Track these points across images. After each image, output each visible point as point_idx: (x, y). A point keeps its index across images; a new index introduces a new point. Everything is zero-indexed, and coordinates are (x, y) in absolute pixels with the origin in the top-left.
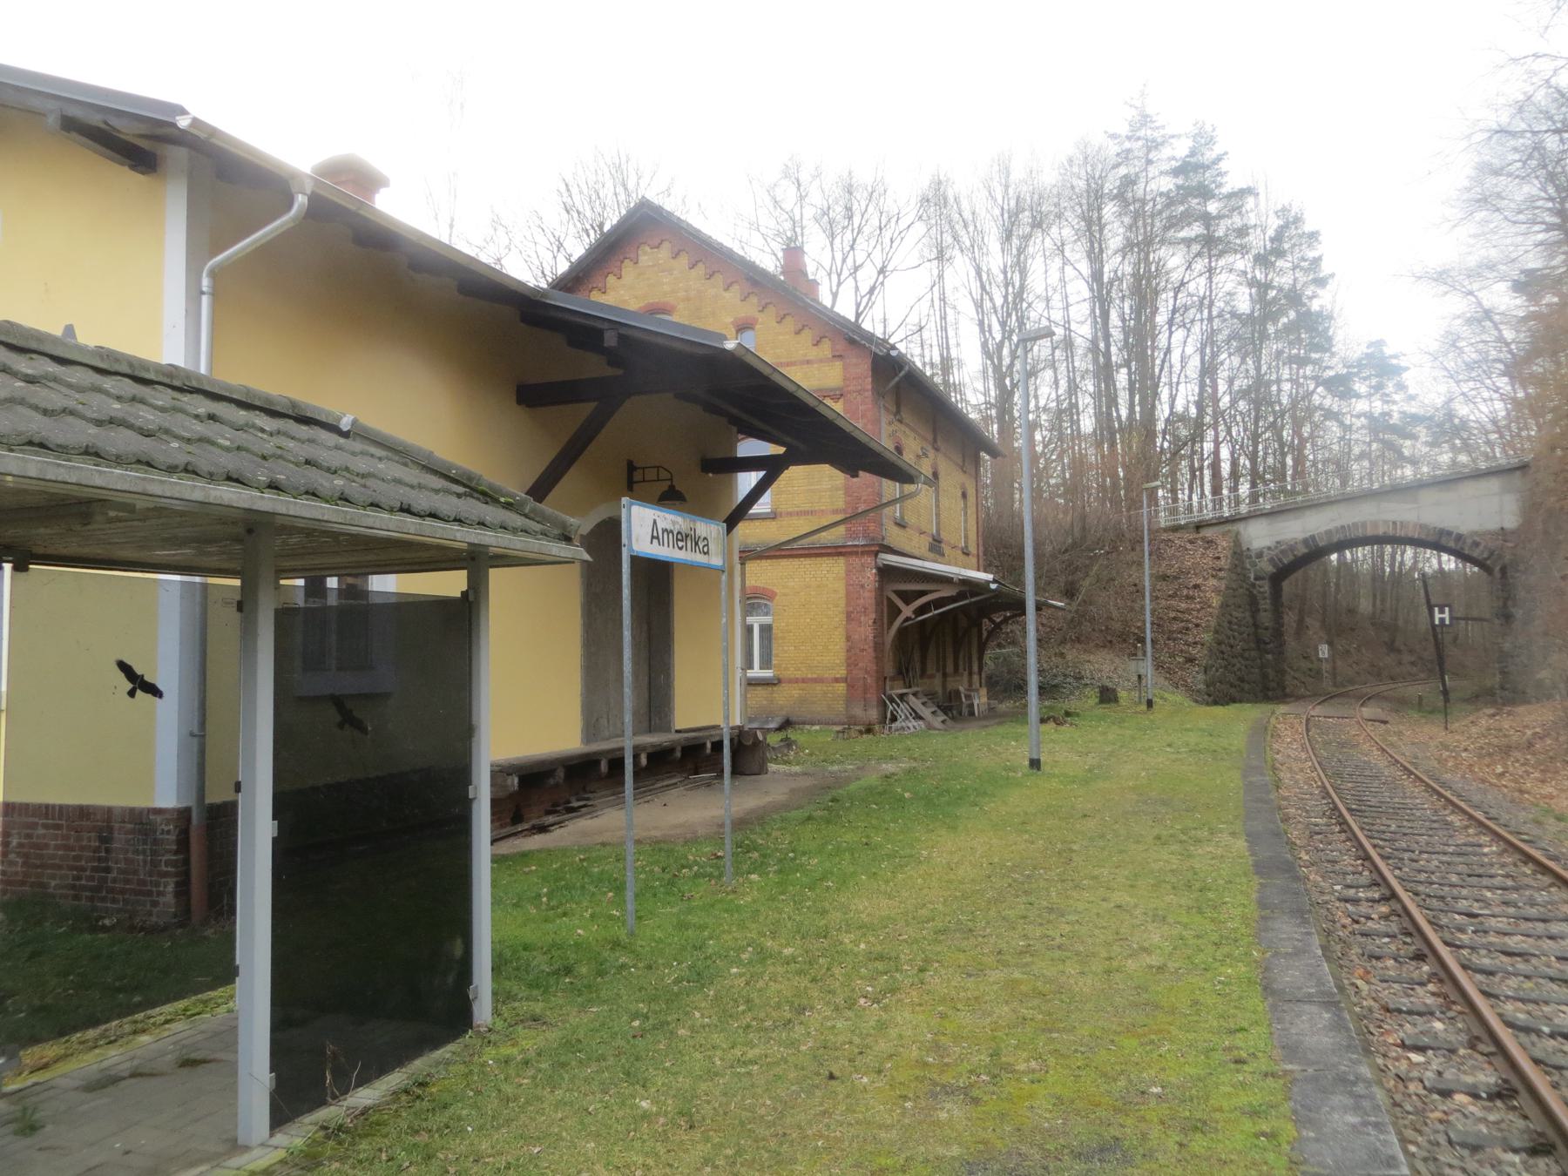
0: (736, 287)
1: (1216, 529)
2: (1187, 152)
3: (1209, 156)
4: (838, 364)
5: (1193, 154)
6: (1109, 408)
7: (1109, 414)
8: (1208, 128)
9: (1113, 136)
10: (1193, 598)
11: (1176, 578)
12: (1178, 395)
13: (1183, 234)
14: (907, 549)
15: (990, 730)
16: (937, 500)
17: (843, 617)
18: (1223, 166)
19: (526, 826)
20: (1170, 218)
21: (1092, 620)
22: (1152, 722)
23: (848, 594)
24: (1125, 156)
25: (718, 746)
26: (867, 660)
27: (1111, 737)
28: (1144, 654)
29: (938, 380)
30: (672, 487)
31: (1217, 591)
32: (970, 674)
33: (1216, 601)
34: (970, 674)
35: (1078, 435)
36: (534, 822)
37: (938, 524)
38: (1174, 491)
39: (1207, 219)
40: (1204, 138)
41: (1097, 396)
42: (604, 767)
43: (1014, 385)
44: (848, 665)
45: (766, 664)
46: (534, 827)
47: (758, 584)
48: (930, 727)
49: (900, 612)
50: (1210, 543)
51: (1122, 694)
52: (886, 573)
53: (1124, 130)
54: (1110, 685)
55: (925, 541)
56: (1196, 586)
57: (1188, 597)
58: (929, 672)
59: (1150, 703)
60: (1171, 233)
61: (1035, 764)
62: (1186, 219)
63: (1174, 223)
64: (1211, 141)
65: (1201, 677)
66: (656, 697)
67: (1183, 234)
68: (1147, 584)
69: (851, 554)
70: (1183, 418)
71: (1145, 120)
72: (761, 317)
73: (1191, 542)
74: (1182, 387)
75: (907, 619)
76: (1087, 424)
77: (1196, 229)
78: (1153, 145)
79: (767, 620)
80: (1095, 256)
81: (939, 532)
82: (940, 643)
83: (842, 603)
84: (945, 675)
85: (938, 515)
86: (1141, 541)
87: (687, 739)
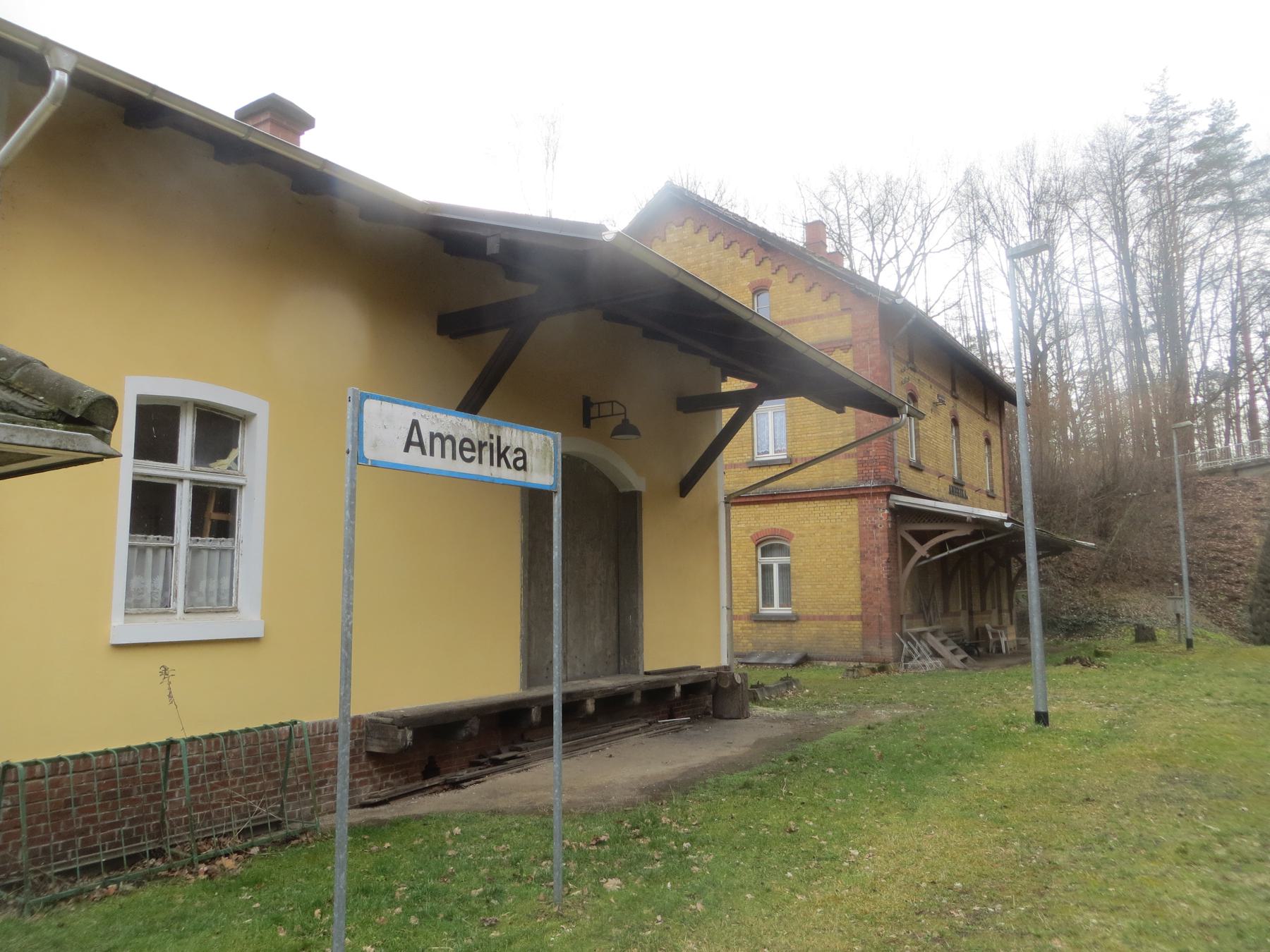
0: (752, 254)
1: (1255, 471)
2: (1207, 128)
3: (1230, 130)
4: (847, 317)
5: (1213, 128)
6: (1140, 363)
7: (1140, 369)
8: (1227, 104)
9: (1134, 119)
10: (1233, 538)
11: (1214, 519)
12: (1210, 354)
13: (1209, 201)
14: (924, 491)
15: (1010, 671)
16: (958, 446)
17: (857, 557)
18: (1245, 137)
19: (436, 781)
20: (1194, 189)
21: (1126, 560)
22: (1192, 663)
23: (861, 534)
24: (1148, 136)
25: (547, 711)
26: (882, 596)
27: (1142, 682)
28: (1182, 594)
29: (975, 353)
30: (625, 421)
31: (1260, 531)
32: (1000, 611)
33: (1258, 541)
34: (1000, 611)
35: (1112, 395)
36: (449, 776)
37: (959, 468)
38: (1211, 442)
39: (1230, 187)
40: (1222, 114)
41: (1128, 356)
42: (535, 715)
43: (1046, 347)
44: (863, 604)
45: (786, 601)
46: (445, 783)
47: (777, 526)
48: (949, 666)
49: (913, 551)
50: (1249, 485)
51: (1161, 633)
52: (900, 514)
53: (1144, 112)
54: (1147, 624)
55: (945, 485)
56: (1236, 527)
57: (1228, 538)
58: (952, 609)
59: (1190, 644)
60: (1195, 202)
61: (1042, 718)
62: (1208, 189)
63: (1196, 192)
64: (1231, 116)
65: (1246, 615)
66: (625, 642)
67: (1209, 201)
68: (1181, 523)
69: (863, 495)
70: (1214, 375)
71: (1166, 101)
72: (774, 279)
73: (1229, 484)
74: (1214, 341)
75: (923, 558)
76: (1120, 380)
77: (1220, 197)
78: (1175, 123)
79: (785, 560)
80: (1121, 230)
81: (960, 472)
82: (958, 578)
83: (856, 543)
84: (971, 613)
85: (959, 460)
86: (1174, 485)
87: (650, 683)
